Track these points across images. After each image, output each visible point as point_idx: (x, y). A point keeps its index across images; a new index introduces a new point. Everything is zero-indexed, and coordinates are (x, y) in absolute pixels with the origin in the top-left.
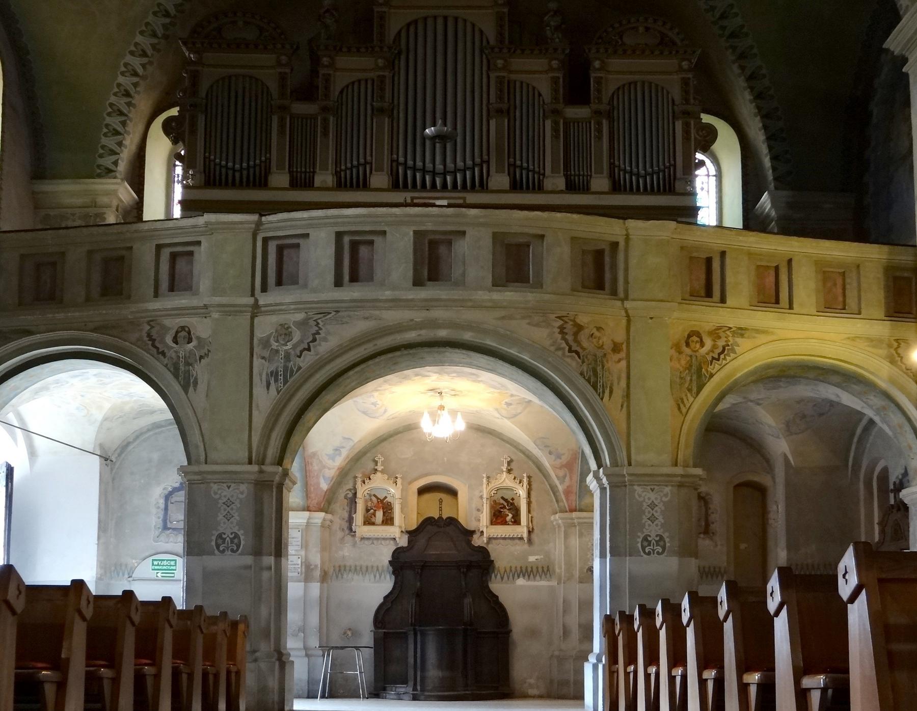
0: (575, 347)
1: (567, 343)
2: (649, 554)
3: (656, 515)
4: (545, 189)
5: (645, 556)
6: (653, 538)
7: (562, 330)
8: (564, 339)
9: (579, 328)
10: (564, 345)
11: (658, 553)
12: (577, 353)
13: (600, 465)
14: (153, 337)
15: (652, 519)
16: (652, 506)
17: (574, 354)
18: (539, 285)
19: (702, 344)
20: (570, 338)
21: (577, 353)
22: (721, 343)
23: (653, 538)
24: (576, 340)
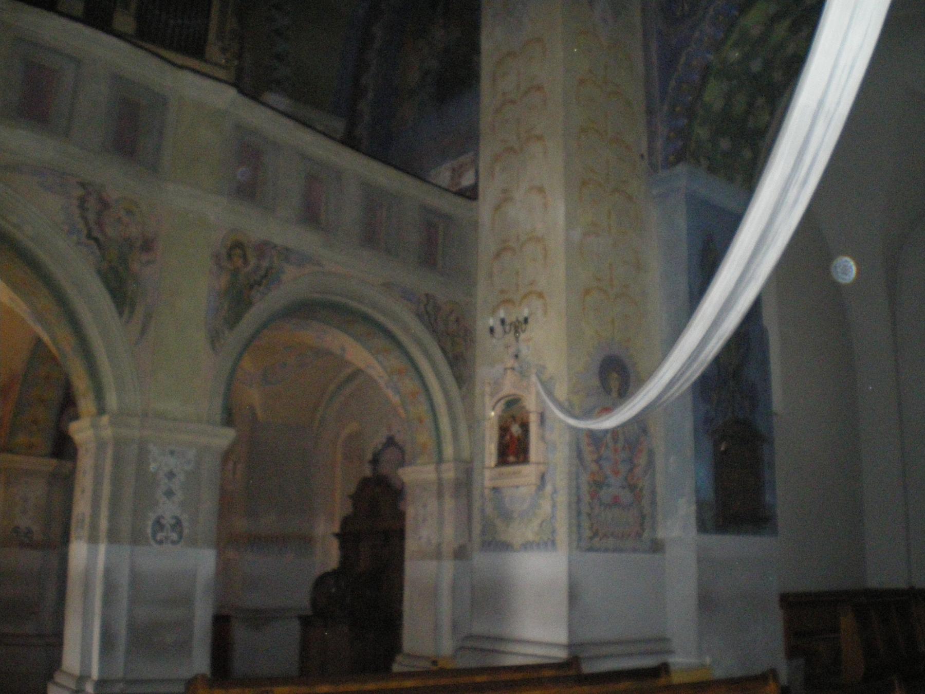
0: (96, 233)
1: (87, 223)
2: (160, 542)
3: (166, 481)
4: (207, 56)
5: (155, 546)
6: (168, 521)
7: (82, 201)
8: (85, 218)
9: (104, 204)
10: (81, 225)
11: (174, 543)
12: (96, 240)
13: (101, 411)
14: (470, 647)
15: (169, 493)
16: (171, 475)
17: (92, 242)
18: (774, 532)
19: (246, 261)
20: (91, 216)
21: (96, 240)
22: (265, 264)
23: (168, 521)
24: (100, 224)
